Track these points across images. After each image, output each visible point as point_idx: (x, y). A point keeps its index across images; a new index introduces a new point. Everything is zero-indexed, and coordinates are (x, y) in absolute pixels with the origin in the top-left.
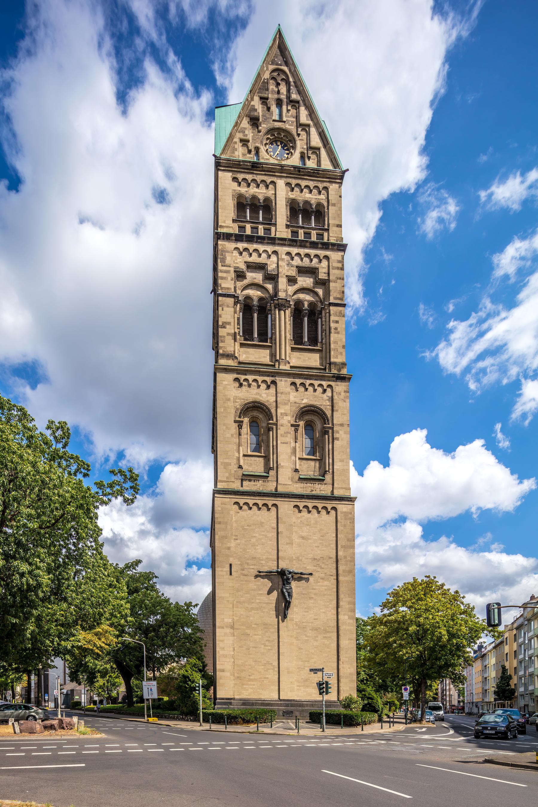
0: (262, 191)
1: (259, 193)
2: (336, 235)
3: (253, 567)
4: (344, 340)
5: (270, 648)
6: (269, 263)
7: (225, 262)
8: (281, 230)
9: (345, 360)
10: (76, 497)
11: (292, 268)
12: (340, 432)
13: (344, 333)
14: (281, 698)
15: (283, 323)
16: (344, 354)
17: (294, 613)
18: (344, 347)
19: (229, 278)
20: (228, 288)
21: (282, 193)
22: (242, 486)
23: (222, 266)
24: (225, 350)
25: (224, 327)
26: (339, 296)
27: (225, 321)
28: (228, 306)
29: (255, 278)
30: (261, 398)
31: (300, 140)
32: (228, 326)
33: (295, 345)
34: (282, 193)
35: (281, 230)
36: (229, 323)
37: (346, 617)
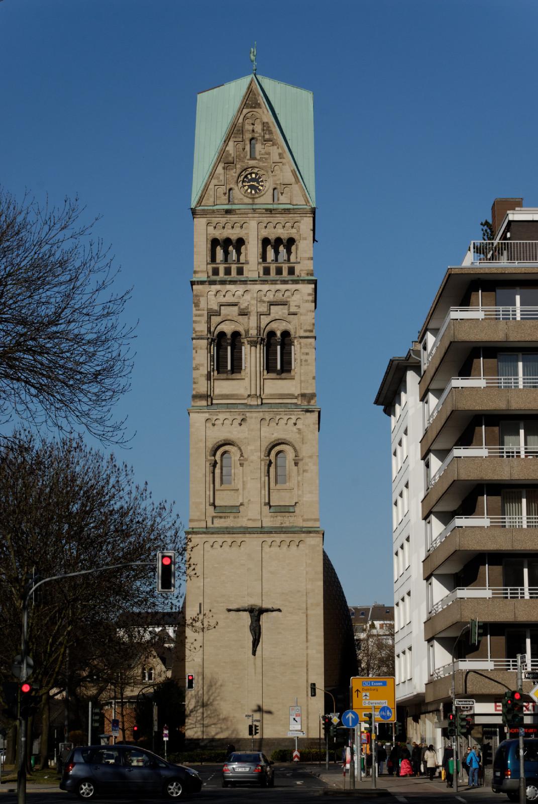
0: (235, 232)
1: (232, 234)
2: (307, 268)
3: (222, 605)
4: (314, 371)
5: (238, 686)
6: (241, 302)
7: (199, 306)
8: (253, 269)
9: (314, 391)
10: (105, 481)
11: (264, 304)
12: (309, 464)
13: (314, 364)
14: (212, 317)
15: (252, 357)
16: (314, 385)
17: (273, 710)
18: (314, 378)
19: (203, 322)
20: (202, 331)
21: (253, 233)
22: (213, 523)
23: (196, 310)
24: (198, 391)
25: (198, 369)
26: (309, 328)
27: (198, 363)
28: (201, 349)
29: (229, 315)
30: (232, 436)
31: (274, 176)
32: (201, 368)
33: (523, 585)
34: (253, 233)
35: (253, 269)
36: (202, 365)
37: (314, 651)
